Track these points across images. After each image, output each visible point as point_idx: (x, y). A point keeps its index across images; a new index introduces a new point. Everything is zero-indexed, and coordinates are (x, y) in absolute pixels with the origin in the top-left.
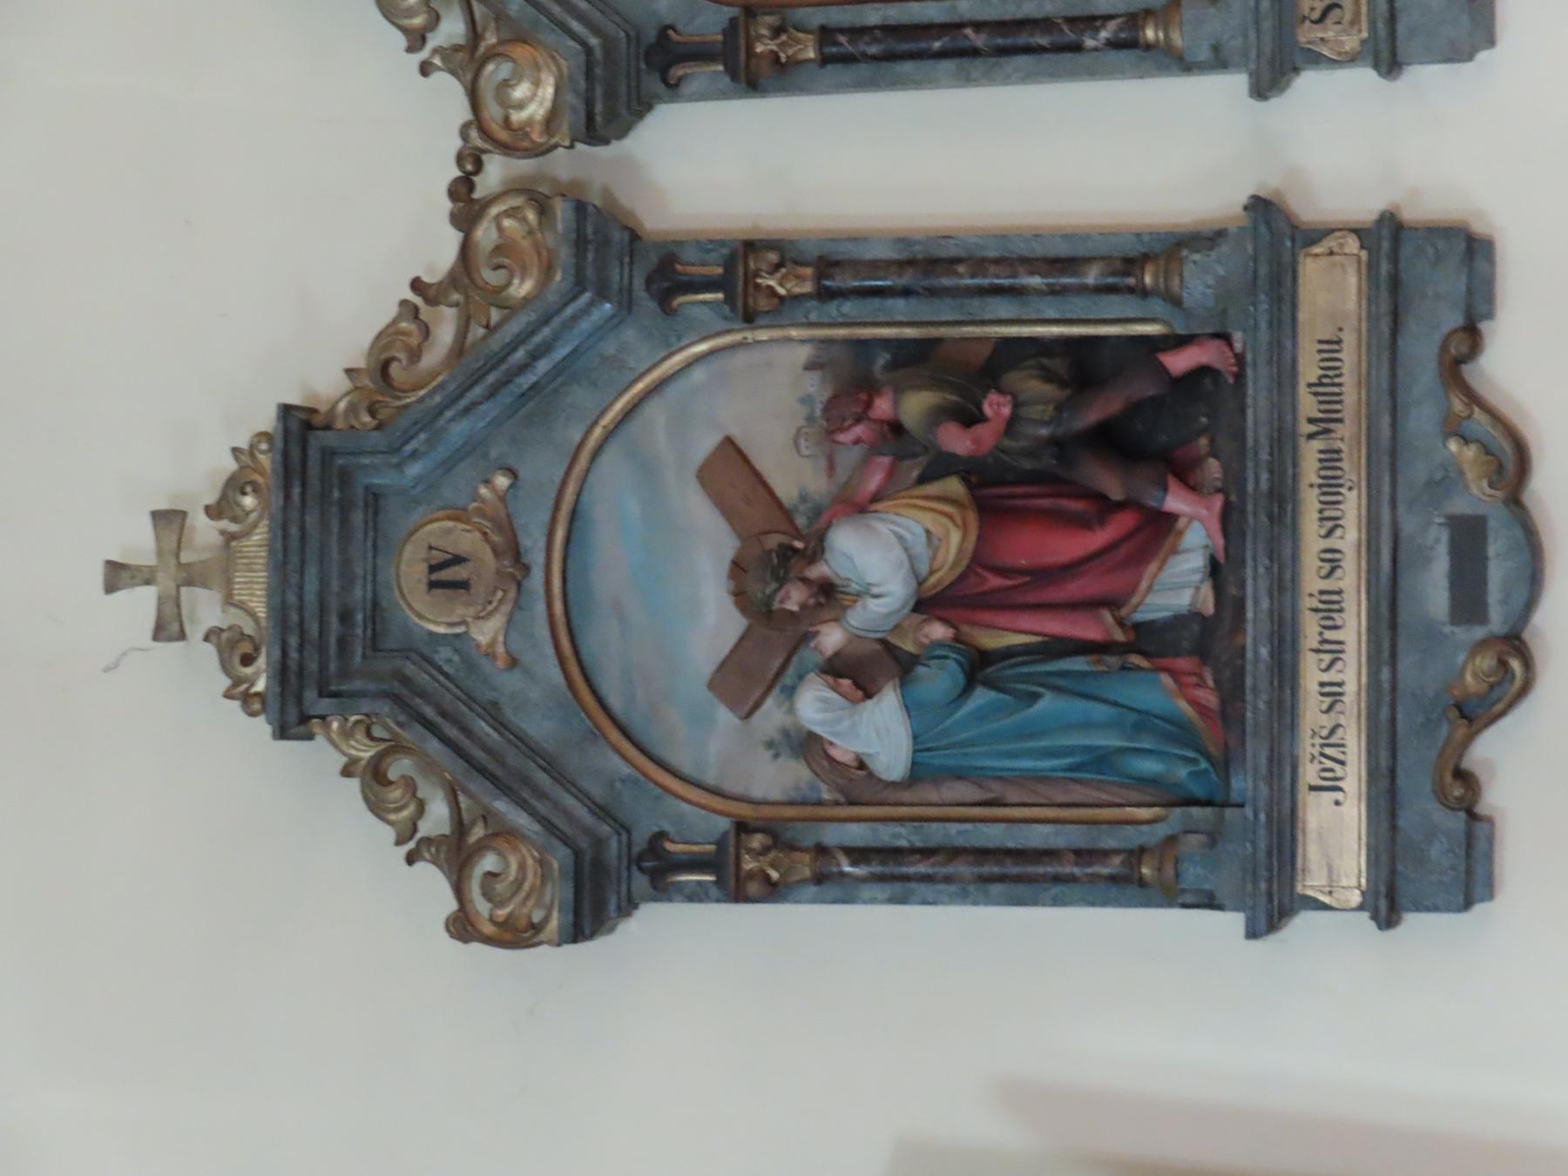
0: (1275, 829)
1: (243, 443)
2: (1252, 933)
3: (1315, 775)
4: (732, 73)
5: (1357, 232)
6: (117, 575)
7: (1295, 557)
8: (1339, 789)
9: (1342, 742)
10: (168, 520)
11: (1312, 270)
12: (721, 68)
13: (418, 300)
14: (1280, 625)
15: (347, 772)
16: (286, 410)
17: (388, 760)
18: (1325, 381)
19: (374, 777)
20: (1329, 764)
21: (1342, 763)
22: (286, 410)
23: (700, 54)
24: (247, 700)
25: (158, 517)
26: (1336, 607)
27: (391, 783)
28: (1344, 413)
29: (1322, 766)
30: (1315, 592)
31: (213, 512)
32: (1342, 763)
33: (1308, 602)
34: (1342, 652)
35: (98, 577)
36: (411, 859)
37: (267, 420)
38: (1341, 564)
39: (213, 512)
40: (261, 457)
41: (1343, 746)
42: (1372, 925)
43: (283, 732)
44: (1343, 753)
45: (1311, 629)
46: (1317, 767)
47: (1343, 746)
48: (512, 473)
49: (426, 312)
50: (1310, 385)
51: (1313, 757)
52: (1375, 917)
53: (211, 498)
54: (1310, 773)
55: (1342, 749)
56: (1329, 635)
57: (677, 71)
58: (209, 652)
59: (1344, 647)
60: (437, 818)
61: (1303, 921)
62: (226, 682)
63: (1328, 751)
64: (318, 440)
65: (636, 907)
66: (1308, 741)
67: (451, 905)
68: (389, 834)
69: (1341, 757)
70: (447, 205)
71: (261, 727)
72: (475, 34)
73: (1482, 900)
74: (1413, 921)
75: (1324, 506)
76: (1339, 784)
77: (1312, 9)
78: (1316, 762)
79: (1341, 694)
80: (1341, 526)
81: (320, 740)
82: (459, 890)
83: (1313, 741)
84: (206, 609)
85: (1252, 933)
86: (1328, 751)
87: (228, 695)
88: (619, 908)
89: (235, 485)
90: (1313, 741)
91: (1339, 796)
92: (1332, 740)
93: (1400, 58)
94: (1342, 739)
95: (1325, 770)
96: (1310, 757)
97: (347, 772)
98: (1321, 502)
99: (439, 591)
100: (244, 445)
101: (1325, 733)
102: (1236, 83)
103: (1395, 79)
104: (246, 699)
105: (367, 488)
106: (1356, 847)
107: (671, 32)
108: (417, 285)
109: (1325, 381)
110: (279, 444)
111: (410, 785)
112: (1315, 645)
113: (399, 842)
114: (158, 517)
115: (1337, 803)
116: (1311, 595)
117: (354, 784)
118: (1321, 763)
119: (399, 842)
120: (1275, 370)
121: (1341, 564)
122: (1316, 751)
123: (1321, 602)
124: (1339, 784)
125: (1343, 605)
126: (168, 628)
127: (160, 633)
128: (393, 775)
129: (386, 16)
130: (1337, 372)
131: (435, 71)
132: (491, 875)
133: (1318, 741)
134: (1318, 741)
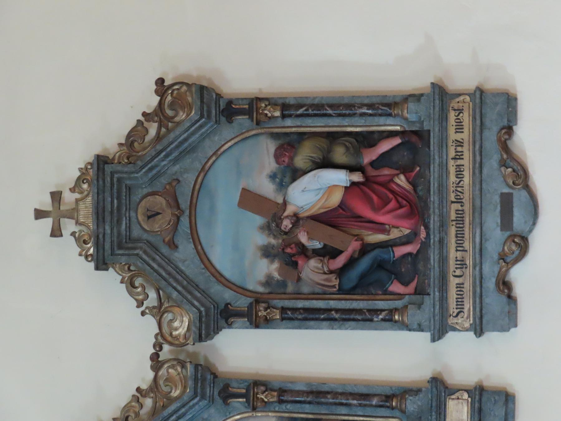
1: (83, 166)
2: (434, 340)
5: (469, 95)
6: (39, 214)
8: (462, 202)
9: (463, 186)
10: (56, 196)
13: (139, 395)
15: (122, 282)
19: (131, 285)
20: (459, 194)
21: (463, 193)
24: (89, 261)
26: (458, 286)
28: (464, 148)
31: (72, 190)
32: (463, 193)
34: (463, 308)
35: (32, 215)
36: (143, 313)
39: (72, 190)
41: (463, 187)
44: (463, 190)
47: (463, 187)
49: (146, 124)
51: (453, 192)
52: (475, 334)
53: (72, 185)
54: (452, 197)
55: (462, 188)
58: (72, 238)
61: (450, 335)
64: (108, 169)
68: (135, 303)
70: (150, 363)
71: (92, 265)
72: (161, 304)
78: (454, 193)
79: (463, 308)
84: (69, 226)
87: (80, 255)
88: (214, 332)
89: (80, 180)
92: (460, 185)
97: (122, 282)
98: (457, 243)
100: (79, 250)
101: (457, 182)
102: (426, 336)
104: (86, 257)
107: (229, 306)
109: (458, 157)
114: (53, 194)
118: (456, 193)
119: (138, 307)
126: (56, 233)
127: (53, 235)
128: (137, 284)
129: (131, 296)
130: (461, 153)
133: (455, 185)
134: (455, 185)
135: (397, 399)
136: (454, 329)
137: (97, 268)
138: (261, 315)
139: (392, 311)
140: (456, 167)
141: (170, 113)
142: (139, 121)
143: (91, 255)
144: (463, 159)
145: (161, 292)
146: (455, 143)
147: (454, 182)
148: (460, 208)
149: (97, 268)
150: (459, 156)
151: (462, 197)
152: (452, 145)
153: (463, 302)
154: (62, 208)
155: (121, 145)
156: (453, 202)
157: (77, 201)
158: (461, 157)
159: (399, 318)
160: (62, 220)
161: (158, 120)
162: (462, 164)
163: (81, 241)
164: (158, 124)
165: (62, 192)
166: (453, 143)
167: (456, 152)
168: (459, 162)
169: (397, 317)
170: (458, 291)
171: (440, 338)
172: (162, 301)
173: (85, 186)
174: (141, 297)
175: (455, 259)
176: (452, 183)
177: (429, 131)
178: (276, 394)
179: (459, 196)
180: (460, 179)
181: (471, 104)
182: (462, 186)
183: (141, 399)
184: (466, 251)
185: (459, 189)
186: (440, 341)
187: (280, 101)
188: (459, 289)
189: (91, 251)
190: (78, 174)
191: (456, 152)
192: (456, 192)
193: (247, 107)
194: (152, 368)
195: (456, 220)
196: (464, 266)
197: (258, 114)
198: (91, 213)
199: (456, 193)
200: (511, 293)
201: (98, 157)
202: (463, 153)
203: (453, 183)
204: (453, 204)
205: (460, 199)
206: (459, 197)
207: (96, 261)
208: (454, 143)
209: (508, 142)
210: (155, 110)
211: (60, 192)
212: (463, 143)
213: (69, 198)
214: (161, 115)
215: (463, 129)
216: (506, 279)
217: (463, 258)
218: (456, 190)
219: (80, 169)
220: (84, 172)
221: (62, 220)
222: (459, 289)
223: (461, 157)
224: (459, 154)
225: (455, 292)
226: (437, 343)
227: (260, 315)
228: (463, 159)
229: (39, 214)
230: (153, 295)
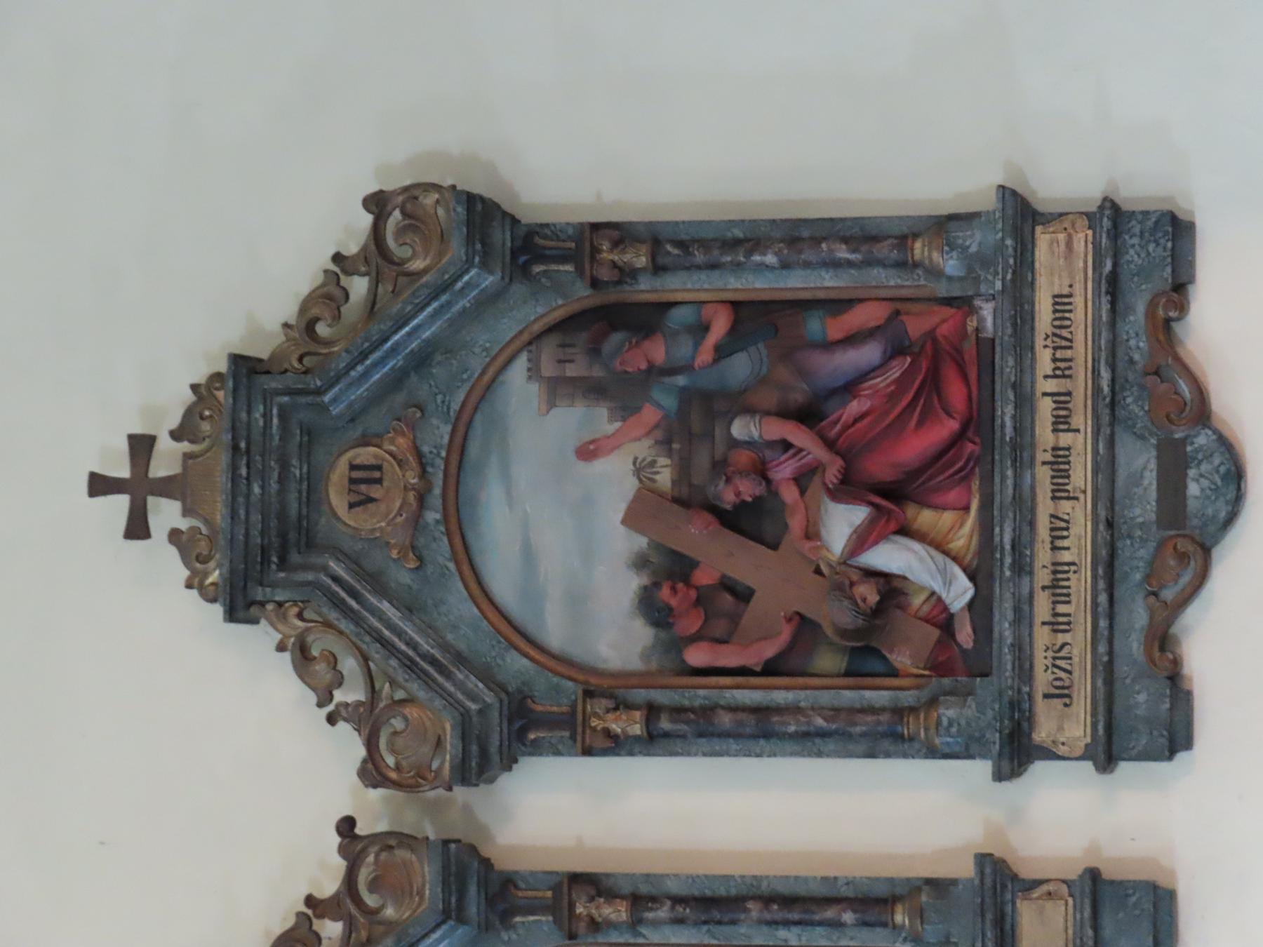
0: (1019, 240)
1: (200, 376)
2: (999, 776)
6: (99, 485)
7: (1032, 667)
10: (141, 446)
11: (1045, 244)
13: (310, 912)
15: (281, 648)
16: (237, 360)
18: (1058, 372)
19: (303, 657)
20: (1063, 675)
21: (1070, 672)
23: (552, 722)
25: (133, 439)
27: (315, 658)
31: (176, 435)
32: (1070, 672)
33: (1041, 456)
39: (176, 435)
41: (1070, 658)
43: (232, 615)
44: (1071, 664)
45: (1042, 607)
47: (1070, 658)
50: (1044, 588)
51: (1047, 667)
53: (174, 421)
55: (1069, 661)
58: (173, 552)
60: (351, 694)
61: (1040, 769)
63: (1059, 662)
65: (516, 761)
67: (361, 752)
68: (312, 698)
69: (1068, 667)
70: (337, 840)
71: (217, 610)
72: (373, 692)
74: (1125, 769)
77: (1054, 645)
78: (1049, 671)
81: (263, 622)
82: (371, 744)
85: (999, 776)
86: (1059, 662)
87: (189, 586)
91: (1067, 701)
92: (1062, 654)
93: (1115, 752)
94: (1069, 653)
95: (1056, 679)
97: (281, 648)
98: (1053, 484)
99: (357, 509)
100: (186, 573)
101: (1057, 647)
102: (981, 769)
103: (1112, 771)
106: (1083, 521)
107: (529, 701)
108: (310, 901)
109: (1058, 372)
111: (333, 661)
112: (1048, 618)
114: (133, 439)
115: (1066, 705)
116: (1044, 567)
117: (287, 656)
118: (1053, 673)
119: (320, 705)
122: (1049, 662)
123: (1057, 688)
126: (137, 528)
132: (395, 733)
134: (1050, 654)
135: (918, 718)
136: (1049, 754)
139: (899, 712)
142: (326, 271)
144: (1070, 377)
146: (1053, 342)
147: (1050, 646)
150: (1063, 370)
151: (1067, 683)
152: (1046, 346)
155: (286, 326)
158: (1067, 372)
160: (151, 500)
161: (374, 339)
166: (1046, 339)
167: (1056, 615)
168: (1065, 439)
170: (1055, 319)
173: (206, 427)
175: (1051, 612)
177: (993, 340)
178: (637, 715)
182: (1069, 655)
183: (344, 280)
184: (1078, 431)
188: (1058, 315)
191: (1055, 360)
192: (1056, 670)
193: (573, 245)
194: (342, 850)
196: (1073, 568)
197: (588, 731)
200: (1181, 669)
202: (1070, 364)
205: (1063, 688)
208: (1049, 340)
209: (1177, 327)
210: (364, 249)
212: (1070, 341)
218: (1055, 666)
219: (195, 388)
221: (151, 500)
222: (1058, 315)
223: (1067, 372)
224: (1062, 365)
225: (1050, 410)
228: (1070, 377)
229: (99, 485)
230: (349, 665)
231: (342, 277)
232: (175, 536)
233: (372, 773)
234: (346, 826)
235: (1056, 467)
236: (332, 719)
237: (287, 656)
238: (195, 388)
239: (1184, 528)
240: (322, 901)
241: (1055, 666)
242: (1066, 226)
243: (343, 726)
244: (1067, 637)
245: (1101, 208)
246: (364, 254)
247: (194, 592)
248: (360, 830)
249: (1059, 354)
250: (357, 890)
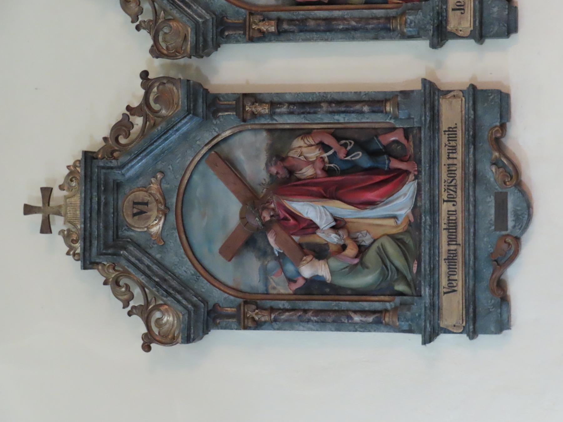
1: (71, 163)
2: (424, 342)
3: (446, 176)
4: (239, 323)
6: (28, 210)
10: (46, 192)
12: (235, 113)
13: (128, 113)
14: (433, 328)
15: (105, 283)
16: (85, 153)
17: (121, 278)
18: (451, 129)
20: (452, 193)
22: (85, 153)
29: (449, 193)
30: (446, 164)
31: (61, 187)
36: (130, 314)
37: (80, 157)
38: (456, 178)
39: (61, 187)
40: (78, 169)
42: (468, 338)
46: (446, 194)
48: (162, 172)
49: (132, 118)
52: (468, 335)
53: (61, 182)
54: (445, 196)
56: (451, 155)
57: (218, 321)
58: (60, 239)
59: (456, 136)
62: (67, 249)
66: (443, 184)
68: (121, 304)
69: (455, 190)
70: (140, 81)
71: (79, 263)
72: (148, 303)
73: (506, 329)
74: (482, 338)
75: (449, 216)
76: (455, 199)
78: (446, 191)
80: (455, 179)
82: (155, 39)
83: (446, 186)
84: (58, 224)
85: (424, 342)
90: (446, 186)
91: (455, 203)
96: (445, 145)
97: (105, 283)
101: (449, 181)
104: (74, 255)
105: (114, 181)
108: (128, 108)
109: (451, 129)
110: (83, 162)
111: (127, 287)
113: (124, 308)
117: (108, 287)
119: (133, 22)
120: (432, 113)
121: (456, 178)
122: (446, 187)
124: (455, 199)
125: (457, 254)
126: (46, 228)
128: (121, 283)
129: (116, 297)
131: (133, 315)
133: (446, 184)
134: (446, 184)
137: (85, 267)
138: (248, 110)
140: (448, 166)
141: (156, 107)
142: (124, 114)
143: (78, 254)
145: (147, 290)
147: (446, 180)
148: (453, 208)
149: (85, 267)
153: (456, 134)
154: (52, 204)
156: (444, 201)
157: (66, 198)
159: (390, 109)
162: (455, 163)
163: (67, 236)
164: (144, 118)
165: (52, 189)
169: (387, 319)
170: (449, 174)
171: (430, 341)
172: (149, 299)
174: (126, 297)
175: (447, 157)
176: (443, 181)
179: (452, 195)
180: (453, 178)
181: (464, 99)
184: (460, 245)
185: (452, 188)
186: (432, 343)
187: (268, 100)
189: (78, 251)
190: (67, 171)
191: (449, 158)
194: (143, 85)
195: (449, 131)
198: (79, 218)
199: (448, 192)
201: (86, 154)
203: (446, 145)
204: (445, 203)
206: (452, 196)
207: (82, 260)
211: (50, 190)
213: (58, 195)
214: (147, 110)
215: (456, 137)
216: (502, 277)
217: (456, 124)
218: (448, 189)
220: (71, 175)
226: (427, 345)
227: (247, 109)
229: (28, 210)
230: (137, 291)
231: (131, 117)
232: (61, 232)
233: (156, 52)
234: (144, 75)
235: (451, 231)
236: (138, 28)
237: (108, 287)
238: (68, 167)
239: (507, 230)
240: (134, 108)
241: (448, 189)
242: (452, 205)
243: (134, 317)
244: (455, 162)
245: (468, 88)
246: (140, 106)
247: (71, 257)
248: (150, 76)
249: (452, 277)
250: (149, 101)
